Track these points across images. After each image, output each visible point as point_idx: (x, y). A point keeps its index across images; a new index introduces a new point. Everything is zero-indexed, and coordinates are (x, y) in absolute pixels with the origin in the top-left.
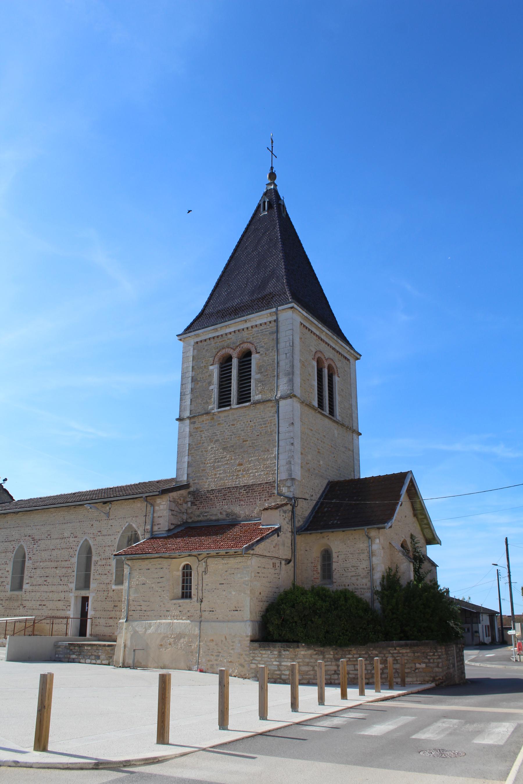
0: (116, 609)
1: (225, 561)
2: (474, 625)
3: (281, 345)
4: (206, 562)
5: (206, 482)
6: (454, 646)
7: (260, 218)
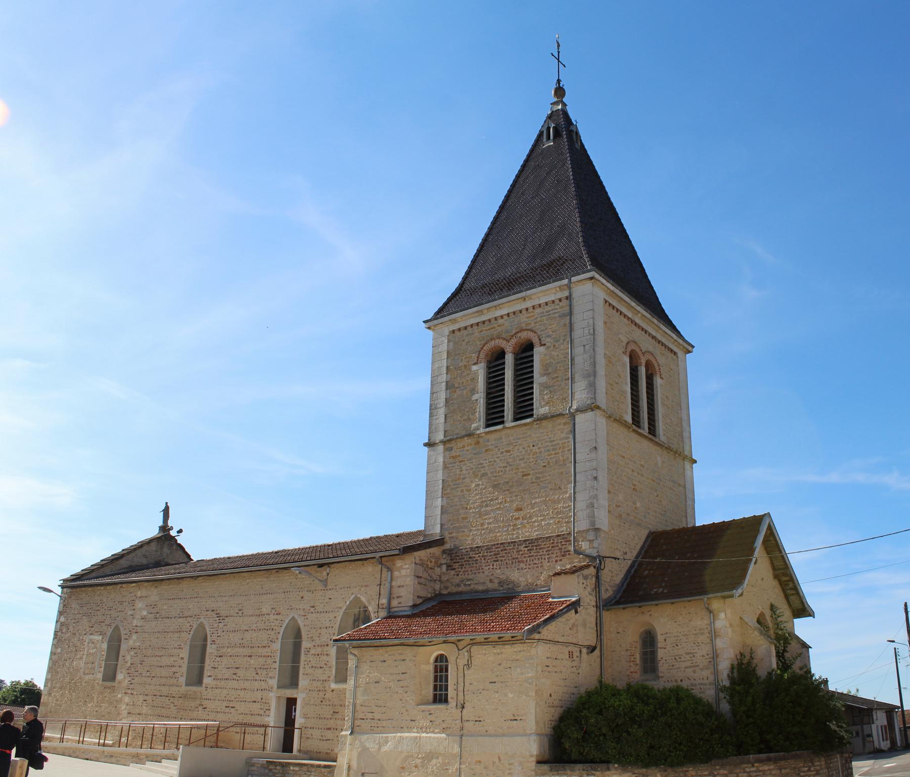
0: (336, 716)
1: (498, 650)
2: (865, 726)
3: (577, 333)
4: (469, 651)
5: (468, 536)
6: (838, 756)
7: (542, 151)
